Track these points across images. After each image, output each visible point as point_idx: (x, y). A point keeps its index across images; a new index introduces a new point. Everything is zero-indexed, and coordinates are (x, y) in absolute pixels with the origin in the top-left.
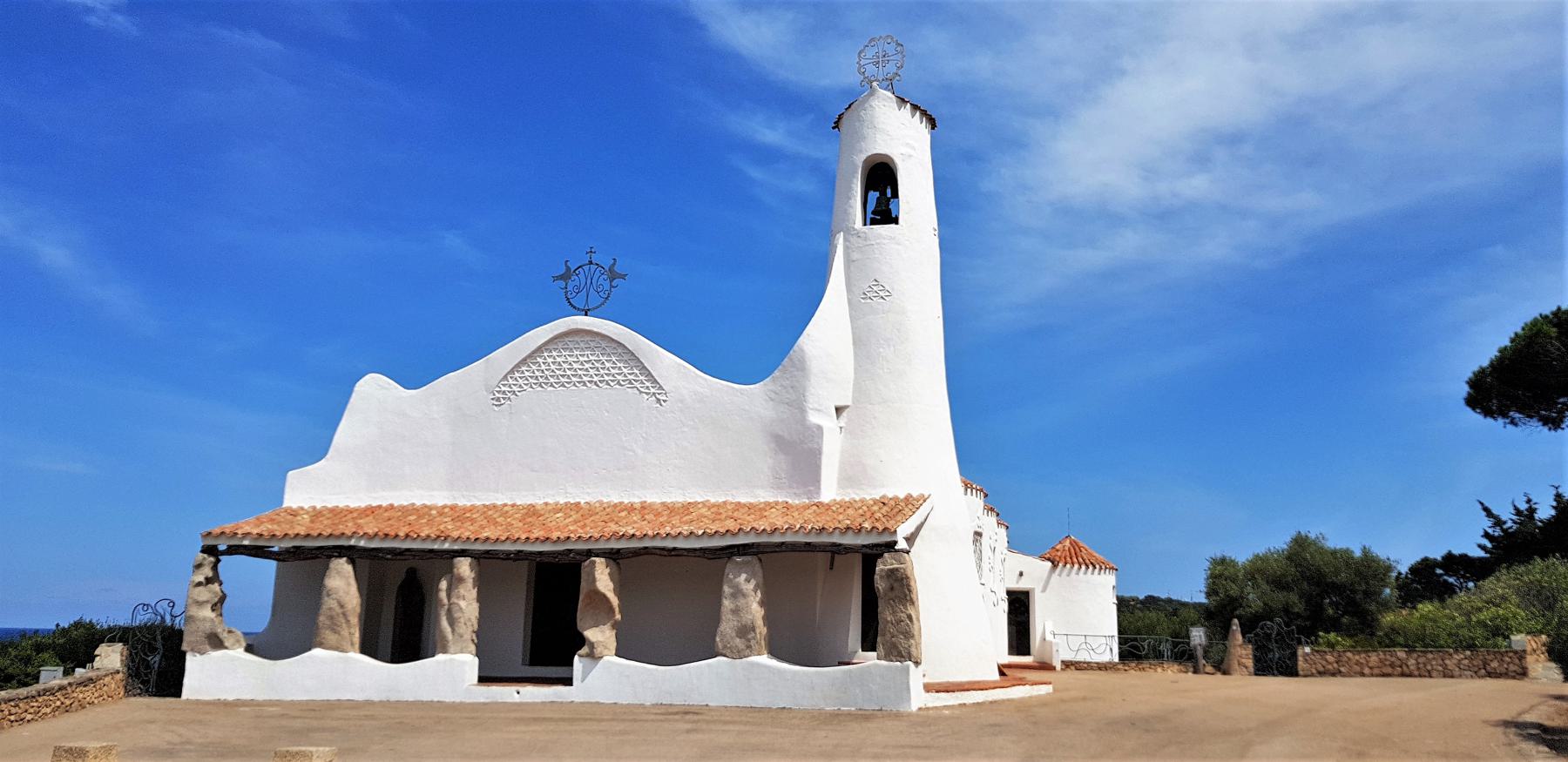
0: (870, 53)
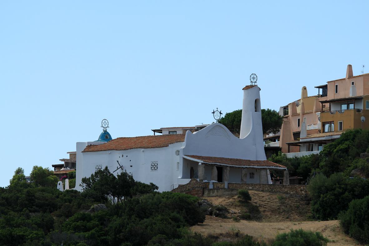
0: (255, 76)
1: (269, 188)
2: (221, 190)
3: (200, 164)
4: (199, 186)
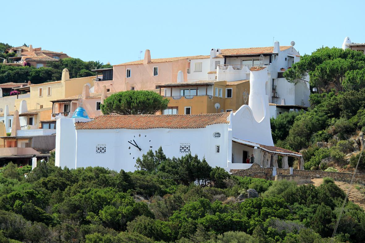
1: (338, 177)
2: (296, 176)
3: (255, 148)
4: (261, 172)
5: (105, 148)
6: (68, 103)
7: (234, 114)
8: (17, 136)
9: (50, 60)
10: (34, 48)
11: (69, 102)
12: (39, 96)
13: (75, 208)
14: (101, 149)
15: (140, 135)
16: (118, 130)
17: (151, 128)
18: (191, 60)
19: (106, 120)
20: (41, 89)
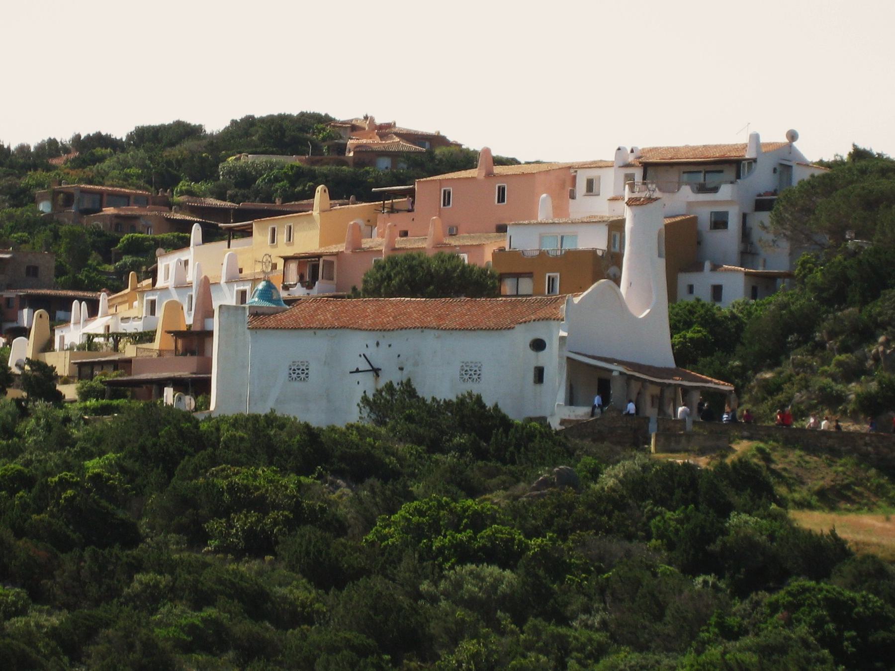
5: (307, 369)
6: (315, 261)
7: (576, 300)
8: (204, 328)
9: (405, 149)
10: (378, 121)
11: (317, 259)
12: (285, 241)
13: (185, 502)
14: (300, 372)
15: (378, 344)
16: (334, 332)
17: (401, 329)
18: (579, 171)
19: (316, 310)
20: (274, 230)
